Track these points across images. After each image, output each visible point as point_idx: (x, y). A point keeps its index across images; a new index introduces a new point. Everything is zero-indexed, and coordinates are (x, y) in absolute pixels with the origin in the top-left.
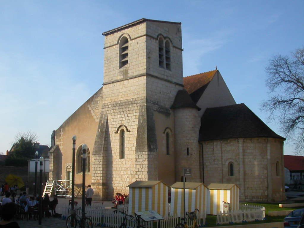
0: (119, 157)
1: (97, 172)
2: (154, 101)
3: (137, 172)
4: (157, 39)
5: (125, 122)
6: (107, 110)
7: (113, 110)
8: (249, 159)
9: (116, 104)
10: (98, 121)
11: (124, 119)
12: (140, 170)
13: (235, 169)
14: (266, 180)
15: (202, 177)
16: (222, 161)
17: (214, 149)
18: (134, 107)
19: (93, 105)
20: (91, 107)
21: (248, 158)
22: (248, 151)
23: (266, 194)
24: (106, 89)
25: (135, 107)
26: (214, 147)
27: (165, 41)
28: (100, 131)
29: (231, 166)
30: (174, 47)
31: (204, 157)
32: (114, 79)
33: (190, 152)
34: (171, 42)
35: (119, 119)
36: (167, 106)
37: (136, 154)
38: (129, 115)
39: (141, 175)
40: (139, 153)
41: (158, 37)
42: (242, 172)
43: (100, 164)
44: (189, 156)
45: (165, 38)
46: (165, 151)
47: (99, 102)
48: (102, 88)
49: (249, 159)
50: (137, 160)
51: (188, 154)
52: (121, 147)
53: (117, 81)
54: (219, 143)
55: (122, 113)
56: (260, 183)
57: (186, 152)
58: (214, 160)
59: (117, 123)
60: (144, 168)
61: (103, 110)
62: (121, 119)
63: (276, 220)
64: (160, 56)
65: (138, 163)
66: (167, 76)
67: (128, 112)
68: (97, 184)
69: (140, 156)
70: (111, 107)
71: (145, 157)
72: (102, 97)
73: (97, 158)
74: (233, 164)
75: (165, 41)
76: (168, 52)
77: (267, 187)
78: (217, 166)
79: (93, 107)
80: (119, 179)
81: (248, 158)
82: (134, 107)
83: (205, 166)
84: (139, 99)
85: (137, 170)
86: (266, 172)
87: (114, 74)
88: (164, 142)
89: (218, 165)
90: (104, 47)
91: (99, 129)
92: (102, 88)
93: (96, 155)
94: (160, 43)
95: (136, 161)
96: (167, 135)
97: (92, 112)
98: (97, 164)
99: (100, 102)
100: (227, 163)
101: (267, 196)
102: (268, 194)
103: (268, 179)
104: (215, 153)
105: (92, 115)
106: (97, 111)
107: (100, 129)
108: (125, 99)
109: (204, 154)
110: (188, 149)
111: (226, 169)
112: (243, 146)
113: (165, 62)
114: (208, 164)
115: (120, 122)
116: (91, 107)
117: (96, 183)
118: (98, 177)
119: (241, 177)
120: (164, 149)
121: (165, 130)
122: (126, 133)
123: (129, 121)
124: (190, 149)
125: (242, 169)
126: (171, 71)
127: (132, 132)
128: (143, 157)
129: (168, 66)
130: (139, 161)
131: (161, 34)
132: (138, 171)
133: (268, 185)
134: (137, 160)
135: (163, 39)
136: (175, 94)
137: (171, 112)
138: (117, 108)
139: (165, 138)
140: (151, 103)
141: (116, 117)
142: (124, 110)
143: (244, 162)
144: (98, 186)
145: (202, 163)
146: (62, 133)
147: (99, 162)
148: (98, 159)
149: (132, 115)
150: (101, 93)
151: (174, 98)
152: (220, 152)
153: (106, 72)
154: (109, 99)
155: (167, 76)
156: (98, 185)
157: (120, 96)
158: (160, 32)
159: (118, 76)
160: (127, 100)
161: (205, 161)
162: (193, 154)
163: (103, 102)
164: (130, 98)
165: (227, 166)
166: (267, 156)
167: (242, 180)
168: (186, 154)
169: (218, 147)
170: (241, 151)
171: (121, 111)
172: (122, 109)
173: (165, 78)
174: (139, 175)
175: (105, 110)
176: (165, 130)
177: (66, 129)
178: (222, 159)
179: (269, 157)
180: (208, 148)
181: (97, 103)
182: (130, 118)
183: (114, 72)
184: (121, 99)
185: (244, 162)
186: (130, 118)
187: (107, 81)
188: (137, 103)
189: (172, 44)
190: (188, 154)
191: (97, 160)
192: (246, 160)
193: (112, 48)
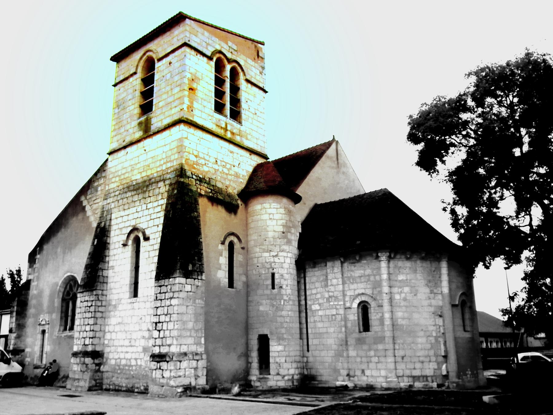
0: (127, 295)
1: (83, 329)
2: (201, 176)
3: (156, 323)
4: (210, 58)
5: (143, 219)
6: (111, 201)
7: (123, 199)
8: (403, 295)
9: (128, 187)
10: (95, 225)
11: (140, 214)
12: (162, 318)
13: (373, 316)
14: (441, 340)
15: (305, 336)
16: (344, 301)
17: (327, 277)
18: (159, 188)
19: (90, 196)
20: (86, 199)
21: (401, 292)
22: (401, 277)
23: (444, 373)
24: (114, 163)
25: (161, 188)
26: (327, 273)
27: (228, 67)
28: (95, 243)
29: (364, 308)
30: (248, 81)
31: (308, 293)
32: (128, 140)
33: (276, 282)
34: (243, 70)
35: (131, 217)
36: (230, 190)
37: (156, 285)
38: (150, 206)
39: (164, 330)
40: (162, 282)
41: (214, 53)
42: (388, 322)
43: (89, 312)
44: (275, 291)
45: (229, 61)
46: (225, 281)
47: (99, 189)
48: (107, 160)
49: (403, 295)
50: (157, 298)
51: (273, 288)
52: (134, 272)
53: (132, 144)
54: (338, 263)
55: (137, 203)
56: (429, 346)
57: (269, 282)
58: (328, 300)
59: (128, 224)
60: (171, 314)
61: (105, 202)
62: (136, 215)
63: (245, 393)
64: (219, 94)
65: (158, 304)
66: (233, 133)
67: (148, 200)
68: (81, 355)
69: (164, 289)
70: (120, 194)
71: (173, 290)
72: (105, 177)
73: (87, 298)
74: (369, 306)
75: (228, 67)
76: (235, 89)
77: (445, 357)
78: (334, 312)
79: (90, 198)
80: (127, 343)
81: (401, 292)
82: (159, 188)
83: (309, 314)
84: (169, 171)
85: (156, 319)
86: (440, 321)
87: (128, 131)
88: (224, 260)
89: (337, 309)
90: (114, 84)
91: (94, 240)
92: (107, 160)
93: (85, 293)
94: (219, 67)
95: (156, 299)
96: (231, 246)
97: (88, 208)
98: (85, 312)
99: (101, 187)
100: (355, 305)
101: (446, 377)
102: (448, 372)
103: (445, 338)
104: (329, 284)
105: (87, 215)
106: (95, 206)
107: (96, 240)
108: (144, 174)
109: (307, 287)
110: (273, 275)
111: (354, 316)
112: (389, 267)
113: (228, 106)
114: (316, 307)
115: (133, 223)
116: (86, 199)
117: (80, 352)
118: (84, 338)
119: (388, 334)
120: (222, 275)
121: (225, 239)
122: (143, 243)
123: (148, 218)
124: (277, 276)
125: (387, 316)
126: (240, 123)
127: (154, 239)
128: (169, 291)
129: (236, 115)
130: (161, 300)
131: (220, 52)
132: (159, 322)
133: (446, 351)
134: (157, 298)
135: (226, 62)
136: (251, 170)
137: (239, 202)
138: (129, 194)
139: (226, 254)
140: (192, 178)
141: (127, 212)
142: (141, 196)
143: (391, 300)
144: (82, 359)
145: (304, 307)
146: (38, 256)
147: (90, 307)
148: (87, 301)
149: (156, 204)
150: (104, 171)
151: (247, 178)
152: (340, 280)
153: (115, 130)
154: (117, 179)
155: (233, 133)
156: (84, 357)
157: (136, 172)
158: (219, 48)
159: (134, 133)
160: (148, 176)
161: (309, 302)
162: (284, 287)
163: (107, 186)
164: (153, 172)
165: (356, 309)
166: (441, 287)
167: (389, 340)
168: (270, 287)
169: (336, 270)
170: (385, 276)
171: (136, 199)
172: (138, 194)
173: (229, 135)
174: (159, 331)
175: (108, 201)
176: (225, 239)
177: (45, 247)
178: (344, 295)
179: (446, 290)
180: (314, 276)
181: (97, 191)
182: (151, 211)
183: (128, 127)
184: (137, 177)
185: (391, 300)
186: (151, 211)
187: (115, 146)
188: (164, 180)
189: (245, 75)
190: (273, 288)
191: (85, 304)
192: (397, 297)
193: (126, 83)
